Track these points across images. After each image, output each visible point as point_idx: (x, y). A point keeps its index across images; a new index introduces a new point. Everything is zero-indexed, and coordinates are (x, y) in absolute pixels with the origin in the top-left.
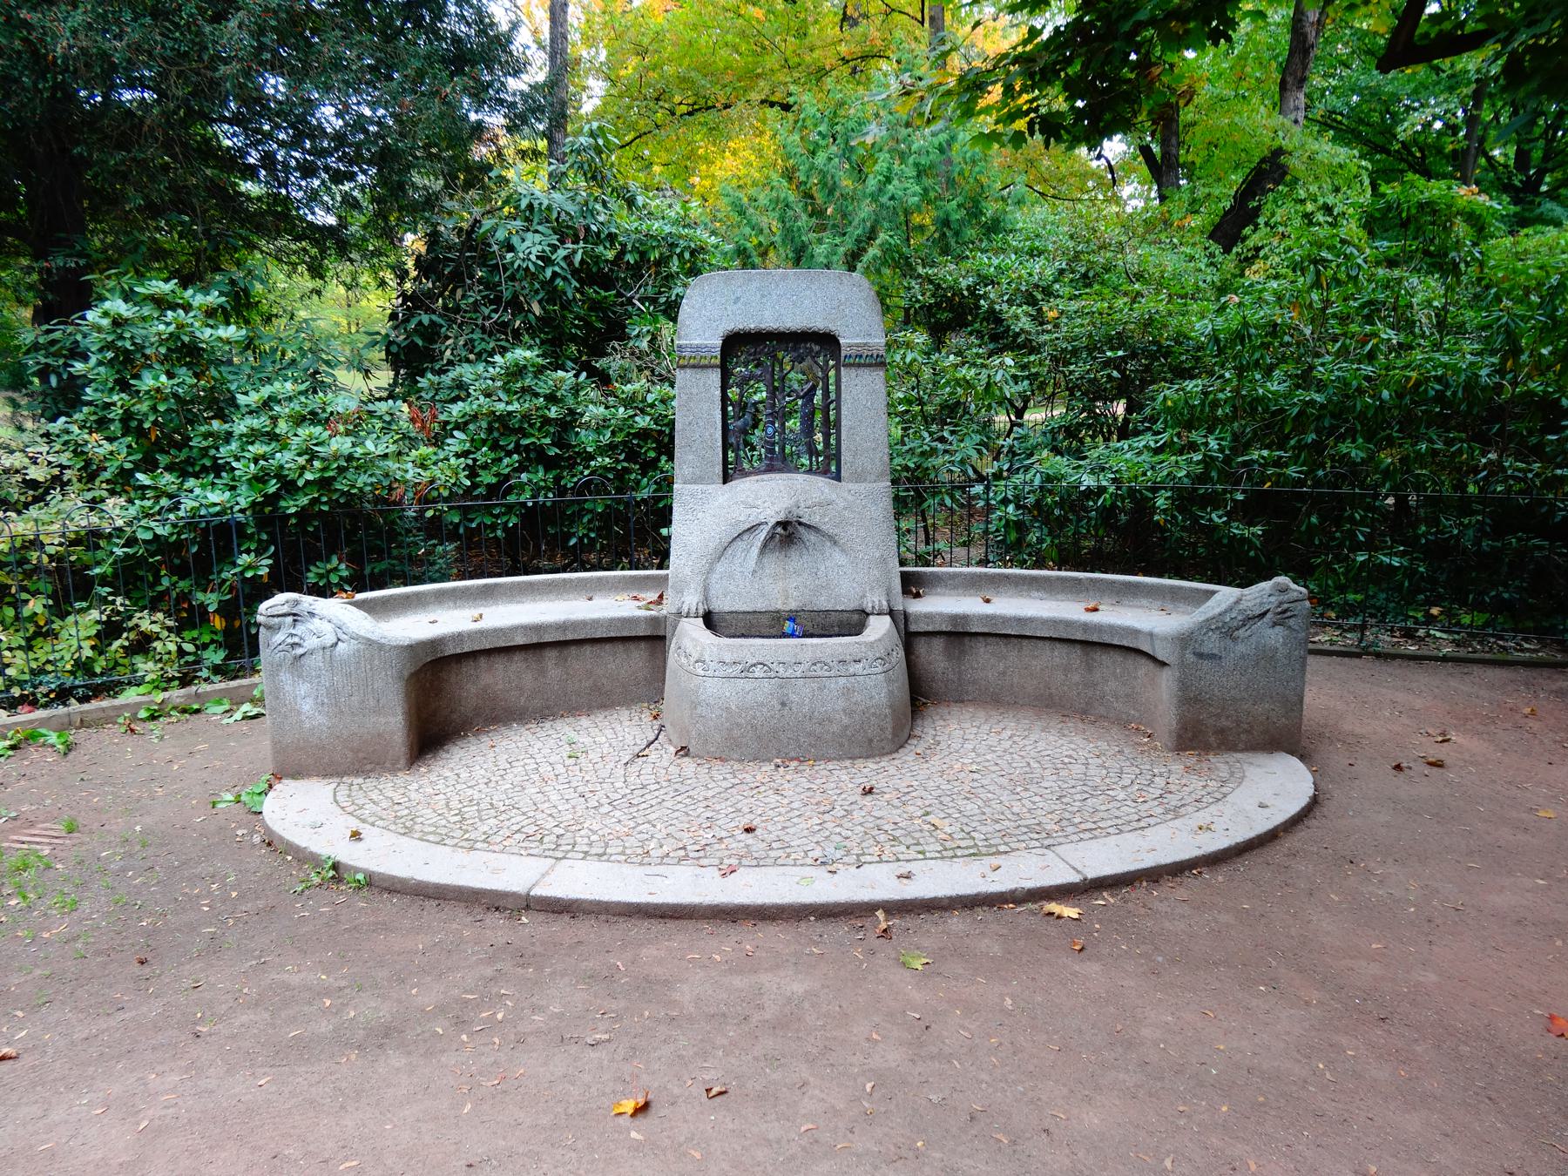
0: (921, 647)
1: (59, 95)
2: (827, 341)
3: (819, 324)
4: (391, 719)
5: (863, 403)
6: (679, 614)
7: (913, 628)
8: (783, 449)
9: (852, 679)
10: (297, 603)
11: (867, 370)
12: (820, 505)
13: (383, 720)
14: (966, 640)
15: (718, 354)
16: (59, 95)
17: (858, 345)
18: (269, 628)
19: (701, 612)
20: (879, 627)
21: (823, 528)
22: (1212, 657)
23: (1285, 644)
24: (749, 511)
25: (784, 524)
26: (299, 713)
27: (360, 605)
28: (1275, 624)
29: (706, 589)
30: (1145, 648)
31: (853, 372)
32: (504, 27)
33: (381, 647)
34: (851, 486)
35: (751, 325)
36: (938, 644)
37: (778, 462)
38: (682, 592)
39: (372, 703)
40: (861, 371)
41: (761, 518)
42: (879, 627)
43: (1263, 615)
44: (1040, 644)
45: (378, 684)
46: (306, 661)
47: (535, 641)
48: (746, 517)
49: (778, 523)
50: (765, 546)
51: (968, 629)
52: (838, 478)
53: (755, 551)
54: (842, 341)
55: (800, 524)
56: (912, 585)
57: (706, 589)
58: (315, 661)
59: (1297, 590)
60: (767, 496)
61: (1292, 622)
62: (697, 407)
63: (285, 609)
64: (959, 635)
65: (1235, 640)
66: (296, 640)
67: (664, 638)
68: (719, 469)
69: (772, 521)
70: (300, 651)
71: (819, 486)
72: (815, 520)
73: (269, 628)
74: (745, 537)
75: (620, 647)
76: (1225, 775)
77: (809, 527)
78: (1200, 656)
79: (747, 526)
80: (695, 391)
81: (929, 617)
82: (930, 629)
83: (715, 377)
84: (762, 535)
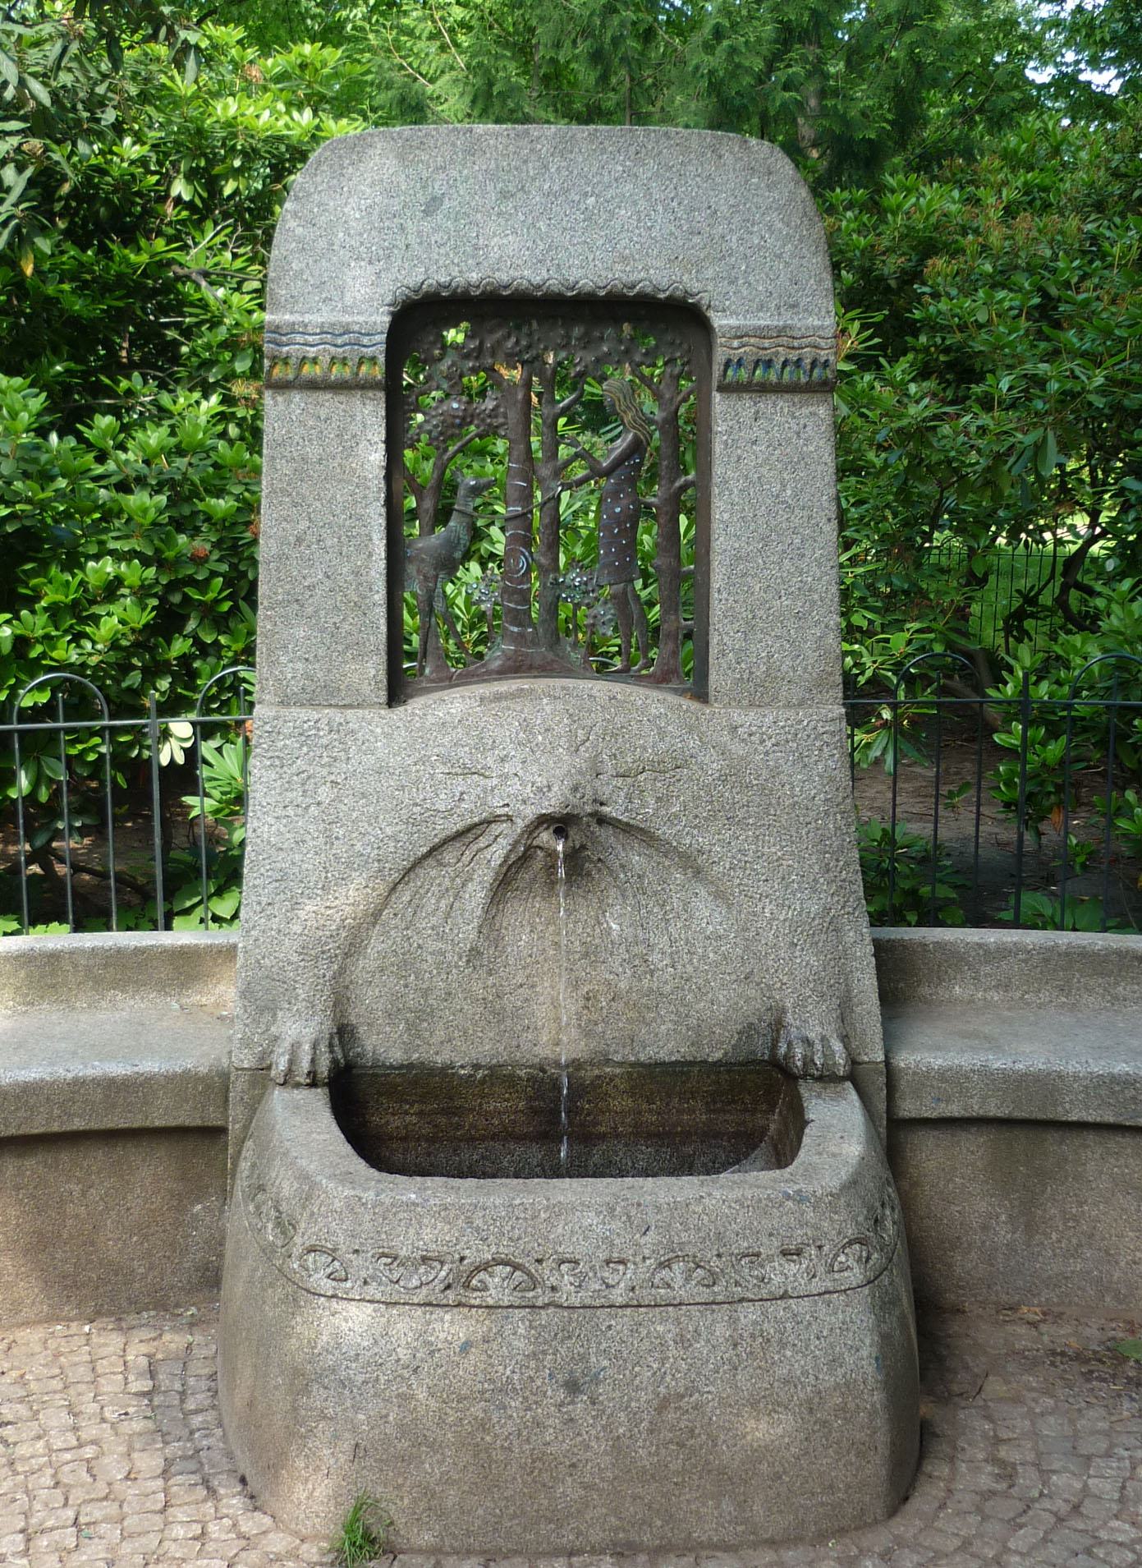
0: (930, 1156)
1: (91, 227)
2: (675, 319)
3: (653, 272)
6: (261, 1075)
7: (908, 1108)
8: (552, 610)
9: (778, 1309)
11: (783, 403)
12: (658, 768)
14: (1052, 1136)
15: (380, 352)
16: (91, 227)
17: (760, 333)
19: (324, 1068)
20: (837, 1133)
21: (664, 831)
24: (460, 785)
25: (561, 824)
29: (340, 1001)
31: (746, 406)
32: (955, 1388)
34: (737, 716)
35: (469, 273)
36: (972, 1148)
37: (536, 640)
38: (274, 1012)
41: (496, 804)
42: (837, 1133)
48: (452, 802)
49: (543, 821)
50: (505, 883)
51: (1059, 1114)
52: (701, 694)
53: (476, 895)
54: (718, 321)
55: (602, 820)
60: (510, 744)
62: (322, 489)
64: (1030, 1129)
67: (221, 1131)
68: (374, 667)
69: (530, 812)
71: (649, 712)
72: (646, 810)
74: (449, 856)
75: (96, 1157)
77: (626, 829)
80: (313, 451)
81: (952, 1079)
82: (955, 1110)
83: (370, 415)
84: (496, 850)
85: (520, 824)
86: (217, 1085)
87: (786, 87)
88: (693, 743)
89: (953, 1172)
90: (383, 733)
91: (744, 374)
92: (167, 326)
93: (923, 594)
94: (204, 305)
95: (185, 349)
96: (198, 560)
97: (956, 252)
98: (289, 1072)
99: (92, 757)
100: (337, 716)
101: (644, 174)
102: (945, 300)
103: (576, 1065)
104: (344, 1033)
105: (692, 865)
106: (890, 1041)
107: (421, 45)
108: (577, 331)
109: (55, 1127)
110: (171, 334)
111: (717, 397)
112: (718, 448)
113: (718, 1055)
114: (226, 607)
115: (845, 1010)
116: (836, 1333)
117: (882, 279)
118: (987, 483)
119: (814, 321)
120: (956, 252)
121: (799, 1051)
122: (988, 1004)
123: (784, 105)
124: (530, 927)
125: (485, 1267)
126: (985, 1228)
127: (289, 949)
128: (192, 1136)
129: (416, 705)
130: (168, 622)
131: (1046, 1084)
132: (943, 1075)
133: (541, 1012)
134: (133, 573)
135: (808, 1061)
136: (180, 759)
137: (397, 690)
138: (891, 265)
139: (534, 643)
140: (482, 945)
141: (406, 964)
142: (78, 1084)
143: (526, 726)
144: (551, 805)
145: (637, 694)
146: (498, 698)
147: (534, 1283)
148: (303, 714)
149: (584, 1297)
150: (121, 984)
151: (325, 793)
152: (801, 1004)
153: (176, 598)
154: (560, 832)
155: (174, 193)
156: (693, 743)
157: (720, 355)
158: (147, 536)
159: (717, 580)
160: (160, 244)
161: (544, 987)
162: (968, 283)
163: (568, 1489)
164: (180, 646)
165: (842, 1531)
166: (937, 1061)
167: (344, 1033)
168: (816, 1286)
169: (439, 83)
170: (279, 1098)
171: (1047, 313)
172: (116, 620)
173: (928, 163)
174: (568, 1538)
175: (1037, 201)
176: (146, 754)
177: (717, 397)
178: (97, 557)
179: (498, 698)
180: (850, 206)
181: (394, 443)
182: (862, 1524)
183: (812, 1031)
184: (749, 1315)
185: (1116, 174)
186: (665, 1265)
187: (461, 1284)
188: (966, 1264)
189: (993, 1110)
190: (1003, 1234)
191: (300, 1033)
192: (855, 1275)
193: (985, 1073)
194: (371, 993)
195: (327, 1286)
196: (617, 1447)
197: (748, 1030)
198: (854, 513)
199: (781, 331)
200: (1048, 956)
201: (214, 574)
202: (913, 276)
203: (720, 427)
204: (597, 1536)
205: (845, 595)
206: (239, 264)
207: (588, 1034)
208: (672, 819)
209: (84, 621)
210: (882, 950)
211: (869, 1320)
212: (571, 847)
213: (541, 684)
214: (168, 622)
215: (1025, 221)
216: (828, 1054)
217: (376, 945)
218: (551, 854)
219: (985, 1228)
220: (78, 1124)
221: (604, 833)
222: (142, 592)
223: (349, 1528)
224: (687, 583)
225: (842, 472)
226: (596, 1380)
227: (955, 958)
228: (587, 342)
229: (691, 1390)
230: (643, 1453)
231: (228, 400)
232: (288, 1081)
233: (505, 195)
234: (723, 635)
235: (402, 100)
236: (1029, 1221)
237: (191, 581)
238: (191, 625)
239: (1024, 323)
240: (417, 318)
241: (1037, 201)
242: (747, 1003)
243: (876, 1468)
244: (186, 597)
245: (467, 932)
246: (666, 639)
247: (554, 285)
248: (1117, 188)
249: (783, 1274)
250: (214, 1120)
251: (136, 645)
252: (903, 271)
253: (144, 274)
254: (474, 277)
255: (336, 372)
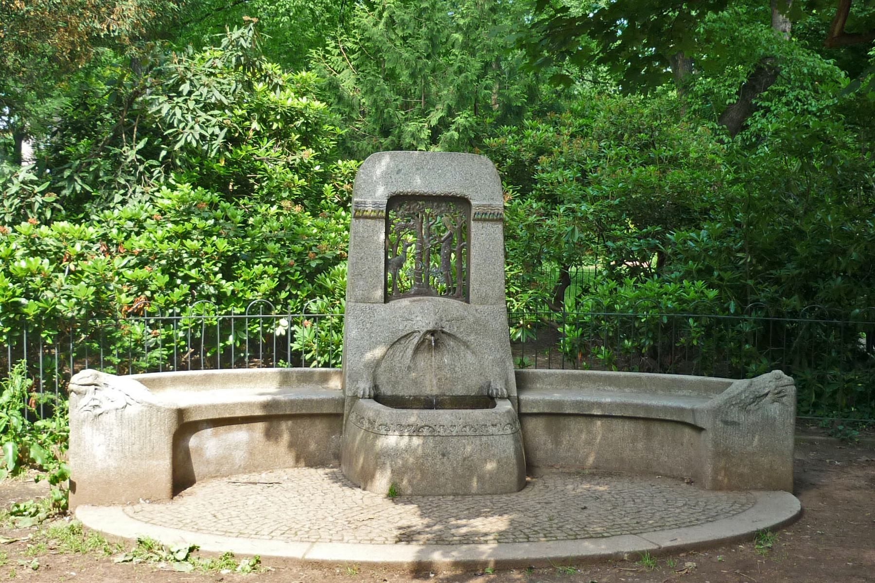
2: (462, 202)
4: (161, 462)
5: (486, 243)
6: (355, 397)
7: (524, 410)
10: (97, 376)
11: (490, 224)
12: (457, 319)
13: (155, 463)
14: (561, 419)
15: (384, 209)
17: (484, 206)
18: (78, 393)
19: (372, 394)
20: (504, 406)
21: (459, 336)
22: (733, 423)
23: (780, 415)
24: (405, 323)
25: (433, 333)
26: (94, 457)
27: (141, 381)
28: (774, 401)
29: (375, 379)
30: (689, 420)
33: (158, 409)
34: (477, 307)
39: (148, 450)
40: (485, 224)
41: (415, 328)
43: (767, 394)
44: (615, 421)
45: (154, 437)
46: (103, 418)
47: (249, 414)
48: (403, 328)
49: (428, 332)
50: (417, 349)
52: (468, 302)
53: (410, 352)
54: (473, 203)
55: (443, 332)
56: (522, 382)
57: (375, 379)
58: (109, 419)
59: (788, 379)
60: (419, 314)
61: (784, 399)
63: (90, 381)
64: (555, 416)
65: (748, 412)
66: (96, 403)
67: (342, 415)
69: (425, 330)
70: (98, 411)
71: (455, 305)
73: (78, 393)
74: (402, 342)
76: (744, 501)
77: (449, 335)
78: (726, 423)
79: (405, 333)
81: (536, 403)
82: (535, 411)
83: (381, 225)
84: (415, 340)
85: (422, 333)
86: (341, 402)
87: (486, 88)
88: (466, 313)
89: (537, 428)
90: (384, 310)
91: (479, 217)
92: (250, 178)
93: (535, 281)
94: (265, 170)
95: (256, 187)
96: (291, 266)
97: (551, 154)
98: (363, 395)
99: (255, 331)
100: (371, 306)
101: (454, 164)
102: (548, 173)
103: (437, 396)
104: (376, 387)
105: (466, 345)
106: (518, 394)
107: (334, 58)
108: (435, 204)
109: (298, 412)
110: (252, 181)
111: (472, 222)
112: (472, 235)
113: (473, 394)
114: (301, 282)
115: (507, 382)
116: (506, 445)
117: (522, 161)
118: (557, 243)
119: (498, 203)
120: (551, 154)
121: (495, 391)
122: (547, 389)
123: (485, 95)
124: (423, 360)
125: (423, 427)
126: (545, 444)
127: (361, 366)
128: (334, 416)
129: (392, 303)
130: (280, 288)
131: (559, 403)
132: (533, 401)
133: (427, 383)
134: (271, 270)
135: (497, 394)
136: (284, 333)
137: (387, 298)
138: (527, 156)
139: (423, 287)
140: (411, 365)
141: (391, 370)
142: (304, 400)
143: (422, 308)
144: (430, 328)
145: (451, 301)
146: (414, 301)
147: (434, 430)
148: (362, 305)
149: (446, 434)
150: (305, 381)
151: (368, 325)
152: (495, 380)
153: (283, 279)
154: (432, 335)
155: (253, 127)
156: (466, 313)
157: (473, 212)
158: (274, 257)
159: (472, 270)
160: (250, 148)
161: (427, 376)
162: (555, 166)
163: (442, 480)
164: (283, 295)
165: (506, 493)
166: (531, 397)
167: (376, 387)
168: (500, 433)
169: (342, 74)
170: (361, 401)
171: (583, 179)
172: (267, 285)
173: (540, 114)
174: (442, 492)
175: (581, 133)
176: (272, 331)
177: (472, 222)
178: (257, 264)
179: (414, 301)
180: (510, 132)
181: (387, 233)
182: (511, 492)
183: (498, 386)
184: (484, 439)
185: (612, 123)
186: (465, 427)
187: (417, 431)
188: (540, 455)
189: (546, 411)
190: (550, 446)
191: (364, 386)
192: (509, 431)
193: (544, 400)
194: (382, 377)
195: (385, 432)
196: (454, 470)
197: (481, 388)
198: (512, 253)
199: (489, 205)
200: (563, 376)
201: (296, 271)
202: (534, 161)
203: (473, 230)
204: (449, 491)
205: (507, 282)
206: (277, 154)
207: (440, 388)
208: (461, 333)
209: (255, 285)
210: (517, 374)
211: (512, 442)
212: (435, 339)
213: (425, 298)
214: (280, 288)
215: (578, 142)
216: (502, 392)
217: (383, 365)
218: (430, 341)
219: (545, 444)
220: (304, 412)
221: (443, 335)
222: (273, 277)
223: (390, 490)
224: (463, 275)
225: (506, 238)
226: (449, 453)
227: (537, 377)
228: (438, 207)
229: (471, 456)
230: (460, 471)
231: (280, 207)
232: (363, 397)
233: (418, 169)
234: (474, 286)
235: (330, 83)
236: (557, 442)
237: (288, 273)
238: (288, 288)
239: (575, 183)
240: (395, 201)
241: (581, 133)
242: (481, 381)
243: (514, 478)
244: (287, 278)
245: (407, 361)
246: (459, 288)
247: (430, 193)
248: (613, 129)
249: (492, 430)
250: (339, 411)
251: (271, 294)
252: (531, 159)
253: (243, 158)
254: (409, 190)
255: (373, 214)
